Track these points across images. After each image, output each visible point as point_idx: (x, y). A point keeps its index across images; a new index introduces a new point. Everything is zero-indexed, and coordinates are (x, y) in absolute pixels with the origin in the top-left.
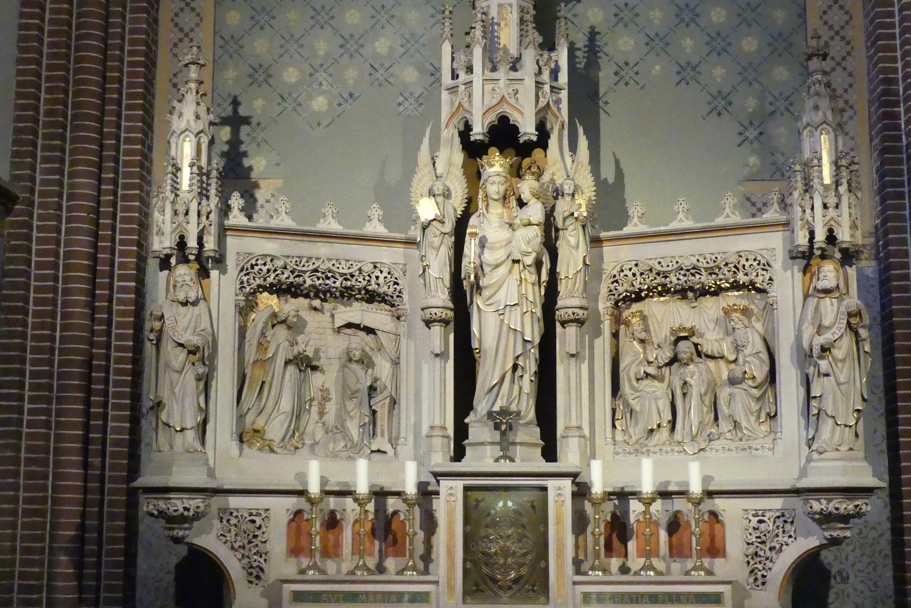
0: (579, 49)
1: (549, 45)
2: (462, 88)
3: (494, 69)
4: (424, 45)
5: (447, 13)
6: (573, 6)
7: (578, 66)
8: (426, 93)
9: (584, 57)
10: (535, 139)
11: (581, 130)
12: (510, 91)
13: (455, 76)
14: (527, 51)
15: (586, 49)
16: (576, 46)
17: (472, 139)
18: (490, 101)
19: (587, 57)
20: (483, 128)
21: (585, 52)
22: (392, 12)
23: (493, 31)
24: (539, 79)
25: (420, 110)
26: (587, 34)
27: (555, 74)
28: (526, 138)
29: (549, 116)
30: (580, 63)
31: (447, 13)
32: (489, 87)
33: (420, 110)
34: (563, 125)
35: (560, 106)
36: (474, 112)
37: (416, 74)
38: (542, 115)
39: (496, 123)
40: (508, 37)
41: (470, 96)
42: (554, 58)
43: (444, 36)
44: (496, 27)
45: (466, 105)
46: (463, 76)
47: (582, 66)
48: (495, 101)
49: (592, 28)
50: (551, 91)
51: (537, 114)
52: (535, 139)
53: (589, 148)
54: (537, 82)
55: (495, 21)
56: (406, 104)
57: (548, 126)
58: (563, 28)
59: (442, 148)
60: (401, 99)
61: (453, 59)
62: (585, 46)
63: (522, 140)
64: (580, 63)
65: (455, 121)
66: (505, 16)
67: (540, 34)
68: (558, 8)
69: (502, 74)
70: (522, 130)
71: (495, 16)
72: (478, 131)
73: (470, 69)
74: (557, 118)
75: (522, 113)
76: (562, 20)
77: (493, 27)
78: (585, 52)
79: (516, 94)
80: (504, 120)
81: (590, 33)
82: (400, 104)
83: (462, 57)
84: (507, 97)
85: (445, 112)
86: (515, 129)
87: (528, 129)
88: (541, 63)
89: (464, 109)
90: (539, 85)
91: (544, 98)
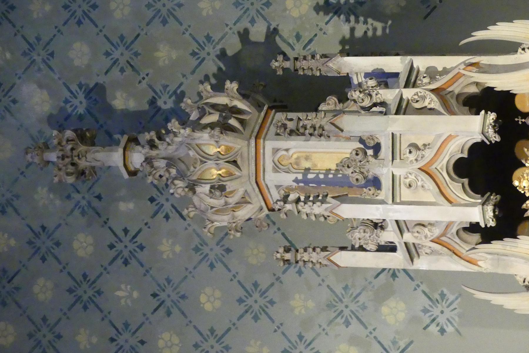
0: (352, 30)
1: (340, 86)
2: (408, 237)
3: (376, 183)
4: (346, 288)
5: (288, 256)
6: (284, 41)
7: (379, 33)
8: (423, 287)
9: (365, 22)
10: (492, 116)
11: (480, 35)
12: (412, 157)
13: (391, 248)
14: (346, 128)
15: (352, 18)
16: (348, 36)
17: (492, 223)
18: (430, 193)
19: (366, 17)
20: (473, 205)
21: (357, 21)
22: (294, 338)
23: (317, 181)
24: (393, 108)
25: (451, 298)
26: (327, 18)
27: (385, 79)
28: (491, 131)
29: (456, 88)
30: (375, 29)
31: (288, 256)
32: (406, 194)
33: (451, 298)
34: (472, 65)
35: (440, 69)
36: (446, 219)
37: (392, 303)
38: (453, 102)
39: (466, 181)
40: (325, 155)
41: (422, 225)
42: (361, 79)
43: (325, 262)
44: (310, 176)
45: (437, 232)
46: (389, 235)
47: (379, 25)
48: (430, 184)
49: (317, 9)
50: (414, 86)
51: (451, 113)
52: (492, 116)
53: (510, 20)
54: (397, 113)
55: (300, 177)
56: (442, 320)
57: (473, 90)
58: (312, 63)
59: (511, 271)
60: (434, 329)
61: (362, 249)
62: (348, 20)
63: (495, 138)
64: (375, 29)
65: (463, 248)
66: (292, 160)
67: (324, 100)
68: (280, 72)
69: (384, 171)
70: (479, 138)
71: (293, 177)
72: (480, 212)
73: (378, 226)
74: (458, 76)
75: (450, 138)
76: (298, 64)
77: (312, 181)
78: (357, 21)
79: (417, 148)
80: (461, 168)
81: (326, 13)
82: (442, 331)
83: (357, 236)
84: (421, 164)
85: (448, 264)
86: (477, 149)
87: (476, 128)
88: (367, 103)
89: (444, 234)
90: (403, 108)
91: (424, 98)
